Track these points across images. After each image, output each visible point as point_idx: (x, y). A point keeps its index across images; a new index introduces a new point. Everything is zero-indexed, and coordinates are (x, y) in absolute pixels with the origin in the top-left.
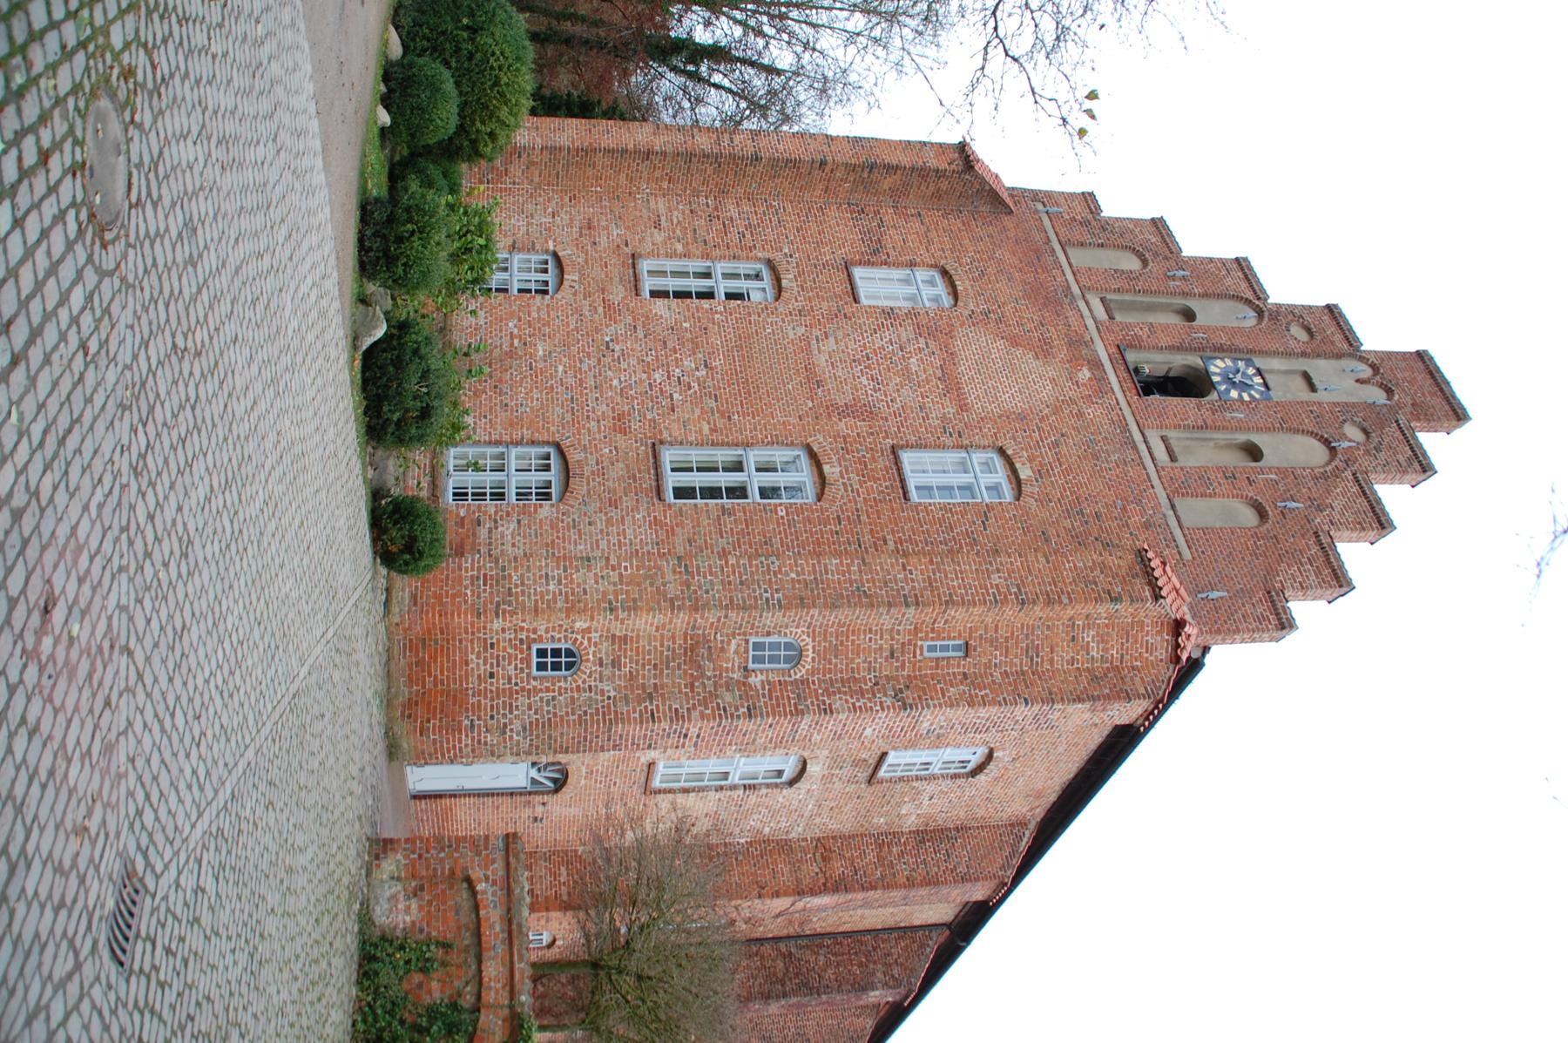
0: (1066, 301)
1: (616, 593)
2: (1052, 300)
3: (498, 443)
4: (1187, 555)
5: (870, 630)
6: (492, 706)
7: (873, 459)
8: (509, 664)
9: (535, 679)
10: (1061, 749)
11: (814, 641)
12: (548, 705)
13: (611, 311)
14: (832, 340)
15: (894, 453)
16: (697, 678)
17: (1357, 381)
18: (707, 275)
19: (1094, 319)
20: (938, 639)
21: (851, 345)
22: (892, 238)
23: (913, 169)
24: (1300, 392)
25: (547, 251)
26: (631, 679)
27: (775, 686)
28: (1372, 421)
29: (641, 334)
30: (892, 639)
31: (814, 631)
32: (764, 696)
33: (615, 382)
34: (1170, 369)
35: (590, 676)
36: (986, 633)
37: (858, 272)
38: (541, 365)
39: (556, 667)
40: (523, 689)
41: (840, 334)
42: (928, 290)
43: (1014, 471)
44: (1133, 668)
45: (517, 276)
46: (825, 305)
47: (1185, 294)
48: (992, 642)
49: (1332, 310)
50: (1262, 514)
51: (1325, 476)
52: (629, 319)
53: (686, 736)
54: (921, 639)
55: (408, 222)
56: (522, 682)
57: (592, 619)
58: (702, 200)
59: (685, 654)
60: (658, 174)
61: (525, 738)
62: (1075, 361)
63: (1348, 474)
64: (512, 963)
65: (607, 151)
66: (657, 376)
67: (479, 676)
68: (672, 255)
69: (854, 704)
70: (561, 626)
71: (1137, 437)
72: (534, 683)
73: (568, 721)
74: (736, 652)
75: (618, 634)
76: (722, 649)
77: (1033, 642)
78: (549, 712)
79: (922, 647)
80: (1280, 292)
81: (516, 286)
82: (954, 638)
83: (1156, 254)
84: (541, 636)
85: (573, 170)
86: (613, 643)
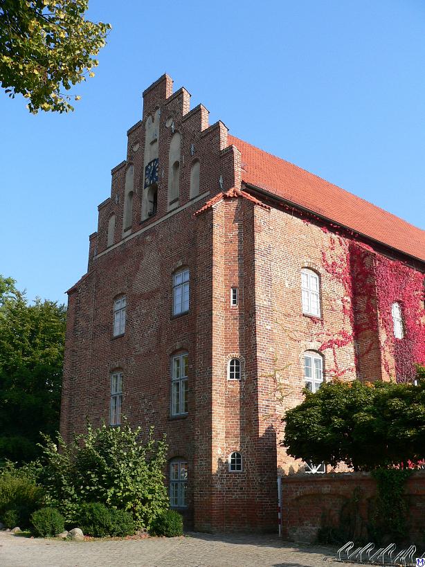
2: (125, 251)
4: (208, 193)
10: (304, 237)
15: (173, 319)
17: (153, 122)
18: (178, 384)
28: (166, 116)
42: (121, 304)
43: (180, 267)
49: (129, 133)
50: (196, 161)
51: (183, 135)
53: (267, 406)
59: (233, 407)
61: (266, 475)
62: (144, 243)
64: (322, 481)
68: (169, 400)
71: (169, 215)
74: (233, 385)
75: (225, 435)
80: (123, 157)
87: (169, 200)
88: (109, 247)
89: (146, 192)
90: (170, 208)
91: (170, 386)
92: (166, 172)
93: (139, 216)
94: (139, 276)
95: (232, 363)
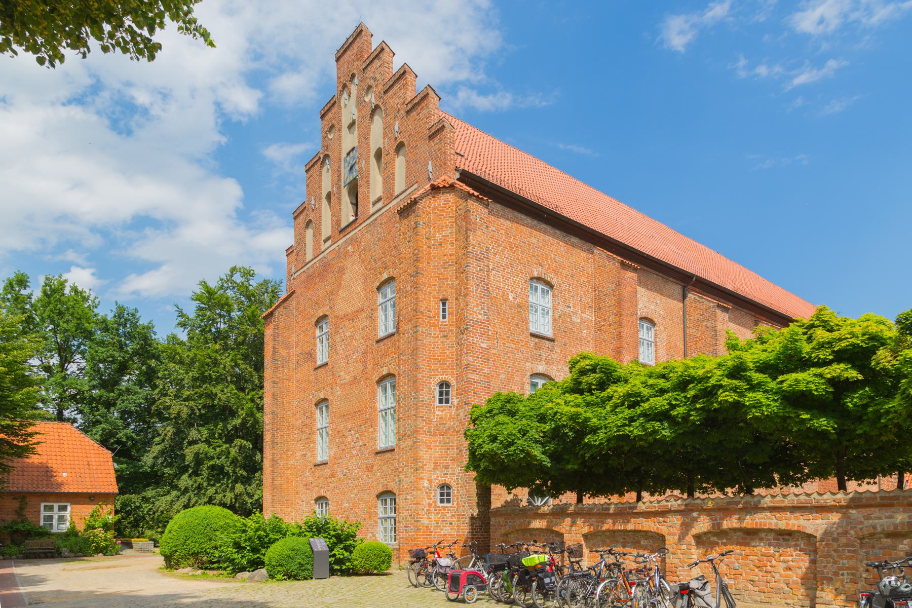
0: (325, 260)
2: (326, 267)
4: (416, 186)
5: (433, 348)
6: (463, 524)
8: (446, 516)
9: (453, 504)
11: (437, 375)
12: (462, 498)
13: (333, 475)
14: (341, 374)
16: (454, 430)
19: (331, 246)
26: (454, 460)
27: (459, 393)
30: (438, 337)
31: (433, 375)
32: (461, 398)
33: (356, 471)
35: (452, 479)
36: (436, 290)
38: (351, 504)
39: (448, 494)
40: (457, 509)
41: (339, 370)
44: (456, 210)
46: (329, 378)
48: (440, 287)
52: (336, 466)
54: (438, 323)
55: (79, 552)
56: (454, 510)
57: (423, 479)
59: (443, 435)
60: (284, 456)
66: (354, 453)
67: (451, 529)
69: (465, 354)
70: (426, 493)
71: (372, 219)
72: (455, 505)
73: (469, 489)
74: (442, 411)
76: (441, 418)
77: (441, 266)
78: (465, 498)
79: (443, 322)
81: (393, 515)
82: (439, 306)
83: (307, 215)
84: (433, 502)
86: (437, 469)
89: (345, 192)
92: (367, 163)
94: (342, 293)
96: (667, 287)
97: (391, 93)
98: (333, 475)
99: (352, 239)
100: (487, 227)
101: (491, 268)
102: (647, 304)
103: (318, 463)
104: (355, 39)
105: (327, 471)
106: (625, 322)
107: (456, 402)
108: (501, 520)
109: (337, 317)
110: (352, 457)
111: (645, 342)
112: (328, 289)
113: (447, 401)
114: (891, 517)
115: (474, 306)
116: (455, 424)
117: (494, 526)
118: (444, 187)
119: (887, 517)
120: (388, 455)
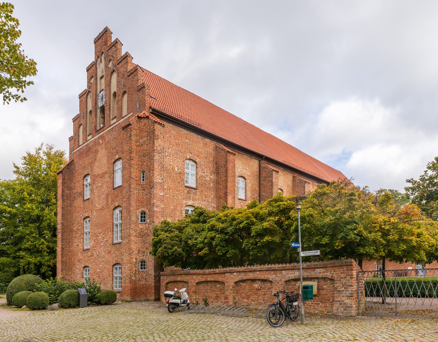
1: (127, 253)
3: (113, 279)
4: (131, 114)
7: (115, 194)
10: (188, 141)
13: (92, 255)
16: (148, 234)
17: (101, 63)
20: (141, 179)
21: (97, 200)
22: (79, 190)
23: (63, 186)
24: (103, 80)
25: (83, 270)
26: (147, 249)
29: (95, 248)
34: (101, 117)
36: (139, 167)
37: (85, 198)
39: (145, 265)
41: (95, 202)
45: (118, 275)
46: (90, 206)
47: (87, 113)
51: (118, 73)
58: (74, 235)
59: (142, 237)
60: (68, 246)
61: (157, 272)
63: (118, 66)
64: (178, 274)
65: (62, 258)
70: (134, 265)
74: (142, 226)
76: (141, 229)
79: (142, 183)
80: (85, 87)
82: (141, 175)
85: (67, 265)
87: (111, 118)
88: (112, 125)
90: (112, 122)
91: (113, 226)
93: (96, 127)
94: (97, 164)
95: (142, 214)
96: (252, 161)
97: (120, 65)
98: (92, 255)
99: (101, 136)
100: (164, 137)
101: (167, 155)
102: (242, 170)
103: (85, 249)
104: (103, 34)
105: (89, 254)
106: (229, 180)
107: (148, 221)
108: (165, 277)
109: (94, 175)
110: (101, 247)
111: (241, 188)
112: (90, 161)
113: (144, 221)
114: (294, 274)
115: (157, 176)
116: (148, 232)
117: (162, 280)
118: (144, 117)
119: (293, 274)
120: (118, 245)
